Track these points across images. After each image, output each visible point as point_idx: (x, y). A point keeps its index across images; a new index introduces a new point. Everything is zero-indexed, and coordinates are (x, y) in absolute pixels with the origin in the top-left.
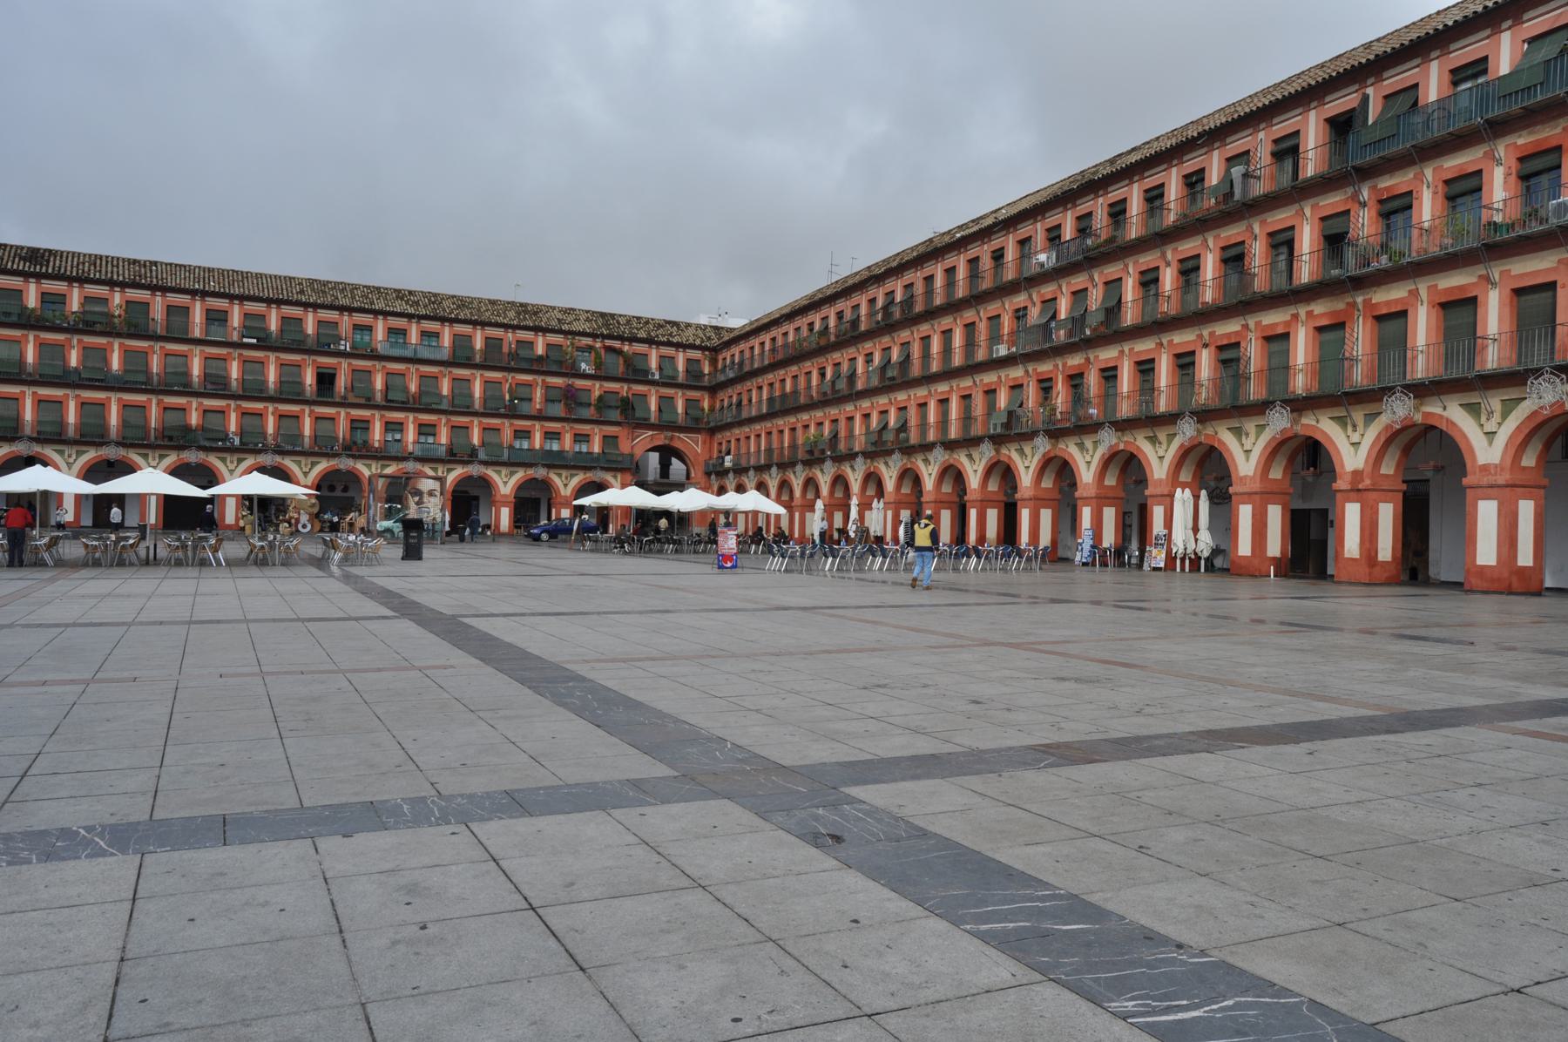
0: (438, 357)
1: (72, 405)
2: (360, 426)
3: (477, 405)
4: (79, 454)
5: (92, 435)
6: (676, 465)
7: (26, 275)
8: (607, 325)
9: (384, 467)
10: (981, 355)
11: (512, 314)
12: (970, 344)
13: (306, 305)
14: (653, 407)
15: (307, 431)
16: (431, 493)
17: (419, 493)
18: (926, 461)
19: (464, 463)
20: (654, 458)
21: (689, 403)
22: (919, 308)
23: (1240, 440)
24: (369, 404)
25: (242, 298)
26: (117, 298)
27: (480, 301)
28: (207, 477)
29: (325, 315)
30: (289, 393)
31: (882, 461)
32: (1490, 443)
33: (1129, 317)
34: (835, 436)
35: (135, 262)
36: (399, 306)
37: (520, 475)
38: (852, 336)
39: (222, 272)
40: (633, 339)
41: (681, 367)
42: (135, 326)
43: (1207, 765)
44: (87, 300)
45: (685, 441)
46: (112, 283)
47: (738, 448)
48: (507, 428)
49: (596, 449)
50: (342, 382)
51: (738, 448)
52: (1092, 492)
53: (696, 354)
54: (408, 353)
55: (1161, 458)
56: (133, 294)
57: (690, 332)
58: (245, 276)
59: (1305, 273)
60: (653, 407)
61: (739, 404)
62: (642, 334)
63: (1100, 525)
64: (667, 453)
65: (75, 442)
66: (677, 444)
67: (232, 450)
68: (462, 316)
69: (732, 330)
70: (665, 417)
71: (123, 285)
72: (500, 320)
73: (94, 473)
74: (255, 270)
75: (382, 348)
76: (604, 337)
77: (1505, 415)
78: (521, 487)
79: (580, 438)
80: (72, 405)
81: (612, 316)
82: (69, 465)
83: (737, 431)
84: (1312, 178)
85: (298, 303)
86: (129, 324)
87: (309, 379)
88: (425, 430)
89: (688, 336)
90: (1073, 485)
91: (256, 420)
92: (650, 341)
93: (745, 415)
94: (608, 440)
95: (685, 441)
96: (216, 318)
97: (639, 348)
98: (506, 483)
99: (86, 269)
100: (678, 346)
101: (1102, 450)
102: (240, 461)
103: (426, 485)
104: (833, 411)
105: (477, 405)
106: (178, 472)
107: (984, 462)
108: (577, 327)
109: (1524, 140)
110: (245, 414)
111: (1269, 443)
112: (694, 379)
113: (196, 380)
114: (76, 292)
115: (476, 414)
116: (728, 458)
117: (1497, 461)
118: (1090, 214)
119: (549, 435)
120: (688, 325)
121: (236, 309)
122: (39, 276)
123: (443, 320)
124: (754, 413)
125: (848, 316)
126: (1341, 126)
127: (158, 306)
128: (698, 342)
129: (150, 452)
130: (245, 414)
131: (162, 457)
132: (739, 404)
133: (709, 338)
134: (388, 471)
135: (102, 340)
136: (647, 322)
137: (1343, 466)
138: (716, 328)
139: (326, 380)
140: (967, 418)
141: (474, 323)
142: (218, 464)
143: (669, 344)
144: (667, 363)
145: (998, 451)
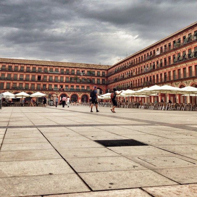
0: (58, 73)
2: (45, 85)
8: (88, 66)
9: (48, 92)
15: (36, 86)
16: (55, 97)
17: (53, 97)
21: (103, 80)
26: (7, 66)
28: (30, 94)
30: (33, 80)
31: (185, 81)
34: (131, 84)
37: (83, 94)
38: (132, 65)
42: (10, 69)
48: (70, 85)
49: (85, 89)
53: (104, 71)
54: (53, 73)
62: (94, 68)
70: (103, 83)
72: (69, 66)
73: (15, 93)
75: (49, 72)
79: (83, 87)
86: (9, 69)
87: (37, 77)
88: (56, 86)
92: (95, 69)
94: (88, 87)
96: (57, 70)
97: (93, 70)
100: (101, 69)
103: (54, 95)
108: (82, 67)
112: (103, 76)
116: (109, 90)
120: (103, 66)
127: (13, 67)
128: (104, 69)
129: (10, 90)
130: (38, 84)
131: (12, 91)
133: (106, 68)
134: (49, 93)
135: (4, 72)
139: (39, 77)
143: (99, 69)
144: (73, 72)
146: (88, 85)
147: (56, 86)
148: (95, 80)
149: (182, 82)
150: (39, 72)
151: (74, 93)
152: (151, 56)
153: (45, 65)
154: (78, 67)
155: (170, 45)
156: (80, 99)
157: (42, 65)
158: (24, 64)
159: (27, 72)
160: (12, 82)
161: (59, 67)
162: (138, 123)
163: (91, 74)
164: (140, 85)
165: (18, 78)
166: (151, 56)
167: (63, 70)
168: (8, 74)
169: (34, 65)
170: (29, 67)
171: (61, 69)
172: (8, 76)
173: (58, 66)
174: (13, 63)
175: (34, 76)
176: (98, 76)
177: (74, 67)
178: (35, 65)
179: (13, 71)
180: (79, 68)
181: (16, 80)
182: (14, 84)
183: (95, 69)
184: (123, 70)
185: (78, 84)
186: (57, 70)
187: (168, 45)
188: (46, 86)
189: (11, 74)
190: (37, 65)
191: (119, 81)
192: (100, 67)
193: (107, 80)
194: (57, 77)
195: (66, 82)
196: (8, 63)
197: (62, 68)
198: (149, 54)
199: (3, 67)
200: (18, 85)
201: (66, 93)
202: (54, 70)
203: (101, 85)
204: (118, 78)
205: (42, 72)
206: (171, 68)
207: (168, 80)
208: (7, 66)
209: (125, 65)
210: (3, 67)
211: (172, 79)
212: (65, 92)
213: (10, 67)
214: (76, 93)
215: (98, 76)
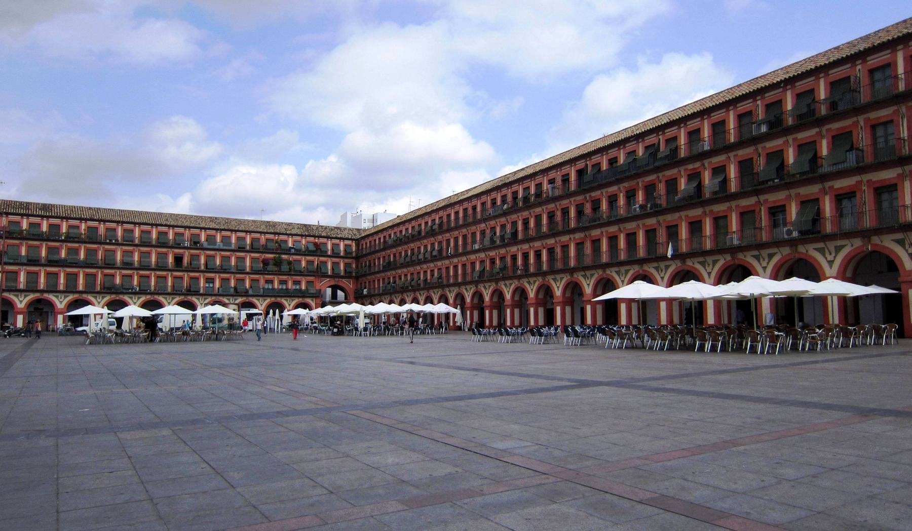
1: (62, 275)
3: (248, 270)
4: (65, 297)
5: (71, 288)
6: (340, 294)
7: (42, 217)
10: (469, 248)
11: (263, 227)
12: (465, 243)
13: (169, 226)
14: (329, 267)
18: (450, 291)
19: (242, 296)
20: (329, 291)
21: (346, 265)
22: (445, 227)
23: (704, 267)
24: (197, 270)
25: (140, 224)
28: (192, 307)
29: (225, 233)
30: (161, 267)
32: (831, 267)
33: (520, 236)
35: (90, 208)
36: (212, 225)
40: (320, 237)
41: (342, 248)
44: (70, 227)
45: (345, 283)
46: (81, 219)
47: (370, 285)
48: (262, 279)
49: (303, 288)
50: (186, 261)
51: (370, 285)
52: (533, 301)
54: (216, 247)
56: (90, 223)
57: (346, 231)
58: (140, 213)
59: (573, 225)
60: (329, 267)
61: (370, 266)
62: (324, 234)
63: (535, 316)
64: (335, 288)
65: (63, 292)
66: (341, 284)
67: (135, 293)
69: (365, 230)
71: (86, 220)
72: (258, 230)
75: (206, 245)
76: (307, 236)
77: (713, 266)
78: (31, 304)
80: (62, 275)
81: (310, 226)
82: (99, 303)
83: (369, 277)
85: (166, 225)
87: (171, 259)
89: (345, 234)
91: (146, 279)
92: (328, 237)
93: (372, 270)
95: (345, 283)
96: (226, 240)
99: (68, 214)
100: (340, 239)
101: (513, 287)
102: (173, 299)
104: (411, 269)
105: (248, 270)
106: (144, 306)
107: (563, 282)
108: (294, 232)
109: (626, 185)
110: (141, 276)
111: (777, 263)
112: (348, 254)
113: (153, 263)
114: (65, 223)
115: (247, 273)
119: (282, 282)
120: (345, 229)
121: (137, 229)
122: (48, 217)
123: (232, 231)
124: (376, 270)
125: (417, 228)
126: (580, 173)
127: (102, 228)
132: (370, 266)
134: (237, 302)
135: (76, 245)
136: (326, 228)
138: (358, 230)
139: (178, 260)
140: (464, 274)
141: (246, 232)
145: (544, 280)
146: (312, 278)
147: (210, 280)
148: (339, 268)
150: (177, 245)
151: (273, 299)
152: (505, 207)
153: (192, 225)
154: (283, 231)
156: (20, 313)
157: (185, 227)
158: (131, 223)
159: (143, 244)
160: (170, 273)
161: (232, 231)
163: (318, 250)
164: (469, 278)
165: (153, 263)
166: (505, 207)
167: (244, 239)
168: (88, 251)
170: (149, 232)
171: (238, 238)
172: (86, 255)
174: (100, 221)
175: (241, 260)
176: (335, 255)
178: (166, 225)
179: (101, 243)
180: (286, 234)
181: (112, 266)
182: (142, 279)
184: (413, 242)
185: (284, 277)
186: (226, 240)
188: (213, 283)
189: (95, 251)
190: (169, 226)
191: (400, 268)
193: (357, 267)
194: (229, 258)
195: (254, 272)
196: (86, 220)
197: (239, 234)
198: (499, 202)
199: (71, 231)
200: (118, 281)
201: (254, 300)
202: (218, 239)
203: (343, 277)
204: (395, 260)
205: (187, 244)
206: (572, 236)
207: (559, 265)
208: (83, 226)
210: (71, 231)
211: (572, 263)
214: (279, 299)
215: (335, 255)
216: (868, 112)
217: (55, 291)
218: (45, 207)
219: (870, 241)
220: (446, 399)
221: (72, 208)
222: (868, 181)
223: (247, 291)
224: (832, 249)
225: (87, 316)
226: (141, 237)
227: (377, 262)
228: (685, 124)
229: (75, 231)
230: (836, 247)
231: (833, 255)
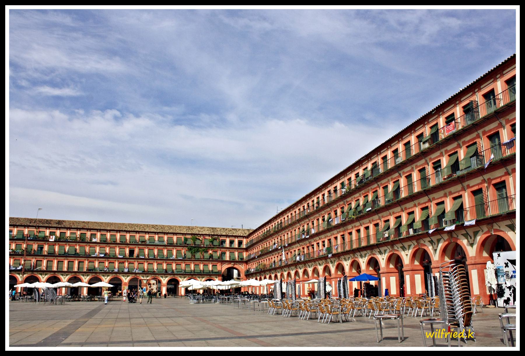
3: (128, 242)
9: (147, 277)
11: (185, 230)
15: (117, 267)
16: (153, 284)
26: (78, 233)
27: (176, 227)
35: (84, 222)
36: (153, 230)
39: (105, 223)
42: (82, 240)
43: (349, 333)
54: (155, 244)
55: (407, 255)
62: (224, 234)
68: (170, 232)
74: (114, 222)
78: (131, 281)
84: (502, 107)
90: (402, 266)
92: (227, 236)
98: (126, 280)
117: (475, 255)
118: (358, 173)
128: (242, 235)
137: (468, 255)
139: (132, 252)
142: (161, 279)
149: (354, 255)
155: (335, 191)
162: (63, 327)
169: (122, 231)
173: (134, 231)
175: (170, 252)
177: (190, 233)
180: (199, 234)
183: (227, 236)
187: (333, 189)
192: (235, 232)
199: (72, 236)
209: (268, 230)
210: (72, 236)
212: (176, 276)
213: (161, 240)
216: (484, 127)
217: (123, 273)
218: (59, 222)
219: (492, 227)
220: (174, 341)
221: (74, 222)
222: (488, 179)
223: (173, 271)
224: (471, 234)
225: (101, 288)
226: (120, 239)
227: (257, 249)
228: (390, 146)
229: (75, 236)
230: (474, 232)
231: (473, 238)
